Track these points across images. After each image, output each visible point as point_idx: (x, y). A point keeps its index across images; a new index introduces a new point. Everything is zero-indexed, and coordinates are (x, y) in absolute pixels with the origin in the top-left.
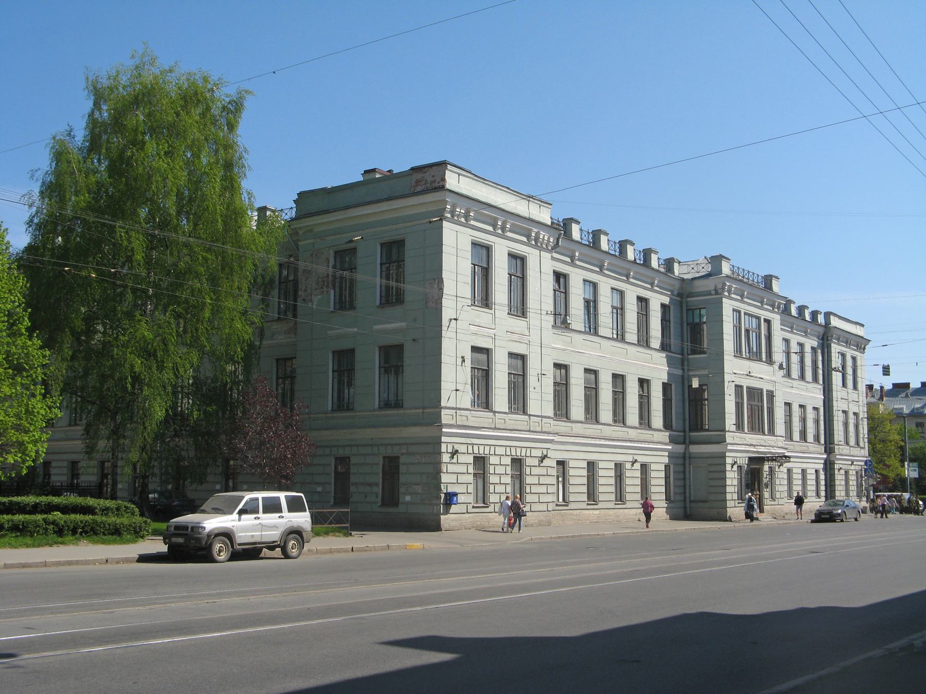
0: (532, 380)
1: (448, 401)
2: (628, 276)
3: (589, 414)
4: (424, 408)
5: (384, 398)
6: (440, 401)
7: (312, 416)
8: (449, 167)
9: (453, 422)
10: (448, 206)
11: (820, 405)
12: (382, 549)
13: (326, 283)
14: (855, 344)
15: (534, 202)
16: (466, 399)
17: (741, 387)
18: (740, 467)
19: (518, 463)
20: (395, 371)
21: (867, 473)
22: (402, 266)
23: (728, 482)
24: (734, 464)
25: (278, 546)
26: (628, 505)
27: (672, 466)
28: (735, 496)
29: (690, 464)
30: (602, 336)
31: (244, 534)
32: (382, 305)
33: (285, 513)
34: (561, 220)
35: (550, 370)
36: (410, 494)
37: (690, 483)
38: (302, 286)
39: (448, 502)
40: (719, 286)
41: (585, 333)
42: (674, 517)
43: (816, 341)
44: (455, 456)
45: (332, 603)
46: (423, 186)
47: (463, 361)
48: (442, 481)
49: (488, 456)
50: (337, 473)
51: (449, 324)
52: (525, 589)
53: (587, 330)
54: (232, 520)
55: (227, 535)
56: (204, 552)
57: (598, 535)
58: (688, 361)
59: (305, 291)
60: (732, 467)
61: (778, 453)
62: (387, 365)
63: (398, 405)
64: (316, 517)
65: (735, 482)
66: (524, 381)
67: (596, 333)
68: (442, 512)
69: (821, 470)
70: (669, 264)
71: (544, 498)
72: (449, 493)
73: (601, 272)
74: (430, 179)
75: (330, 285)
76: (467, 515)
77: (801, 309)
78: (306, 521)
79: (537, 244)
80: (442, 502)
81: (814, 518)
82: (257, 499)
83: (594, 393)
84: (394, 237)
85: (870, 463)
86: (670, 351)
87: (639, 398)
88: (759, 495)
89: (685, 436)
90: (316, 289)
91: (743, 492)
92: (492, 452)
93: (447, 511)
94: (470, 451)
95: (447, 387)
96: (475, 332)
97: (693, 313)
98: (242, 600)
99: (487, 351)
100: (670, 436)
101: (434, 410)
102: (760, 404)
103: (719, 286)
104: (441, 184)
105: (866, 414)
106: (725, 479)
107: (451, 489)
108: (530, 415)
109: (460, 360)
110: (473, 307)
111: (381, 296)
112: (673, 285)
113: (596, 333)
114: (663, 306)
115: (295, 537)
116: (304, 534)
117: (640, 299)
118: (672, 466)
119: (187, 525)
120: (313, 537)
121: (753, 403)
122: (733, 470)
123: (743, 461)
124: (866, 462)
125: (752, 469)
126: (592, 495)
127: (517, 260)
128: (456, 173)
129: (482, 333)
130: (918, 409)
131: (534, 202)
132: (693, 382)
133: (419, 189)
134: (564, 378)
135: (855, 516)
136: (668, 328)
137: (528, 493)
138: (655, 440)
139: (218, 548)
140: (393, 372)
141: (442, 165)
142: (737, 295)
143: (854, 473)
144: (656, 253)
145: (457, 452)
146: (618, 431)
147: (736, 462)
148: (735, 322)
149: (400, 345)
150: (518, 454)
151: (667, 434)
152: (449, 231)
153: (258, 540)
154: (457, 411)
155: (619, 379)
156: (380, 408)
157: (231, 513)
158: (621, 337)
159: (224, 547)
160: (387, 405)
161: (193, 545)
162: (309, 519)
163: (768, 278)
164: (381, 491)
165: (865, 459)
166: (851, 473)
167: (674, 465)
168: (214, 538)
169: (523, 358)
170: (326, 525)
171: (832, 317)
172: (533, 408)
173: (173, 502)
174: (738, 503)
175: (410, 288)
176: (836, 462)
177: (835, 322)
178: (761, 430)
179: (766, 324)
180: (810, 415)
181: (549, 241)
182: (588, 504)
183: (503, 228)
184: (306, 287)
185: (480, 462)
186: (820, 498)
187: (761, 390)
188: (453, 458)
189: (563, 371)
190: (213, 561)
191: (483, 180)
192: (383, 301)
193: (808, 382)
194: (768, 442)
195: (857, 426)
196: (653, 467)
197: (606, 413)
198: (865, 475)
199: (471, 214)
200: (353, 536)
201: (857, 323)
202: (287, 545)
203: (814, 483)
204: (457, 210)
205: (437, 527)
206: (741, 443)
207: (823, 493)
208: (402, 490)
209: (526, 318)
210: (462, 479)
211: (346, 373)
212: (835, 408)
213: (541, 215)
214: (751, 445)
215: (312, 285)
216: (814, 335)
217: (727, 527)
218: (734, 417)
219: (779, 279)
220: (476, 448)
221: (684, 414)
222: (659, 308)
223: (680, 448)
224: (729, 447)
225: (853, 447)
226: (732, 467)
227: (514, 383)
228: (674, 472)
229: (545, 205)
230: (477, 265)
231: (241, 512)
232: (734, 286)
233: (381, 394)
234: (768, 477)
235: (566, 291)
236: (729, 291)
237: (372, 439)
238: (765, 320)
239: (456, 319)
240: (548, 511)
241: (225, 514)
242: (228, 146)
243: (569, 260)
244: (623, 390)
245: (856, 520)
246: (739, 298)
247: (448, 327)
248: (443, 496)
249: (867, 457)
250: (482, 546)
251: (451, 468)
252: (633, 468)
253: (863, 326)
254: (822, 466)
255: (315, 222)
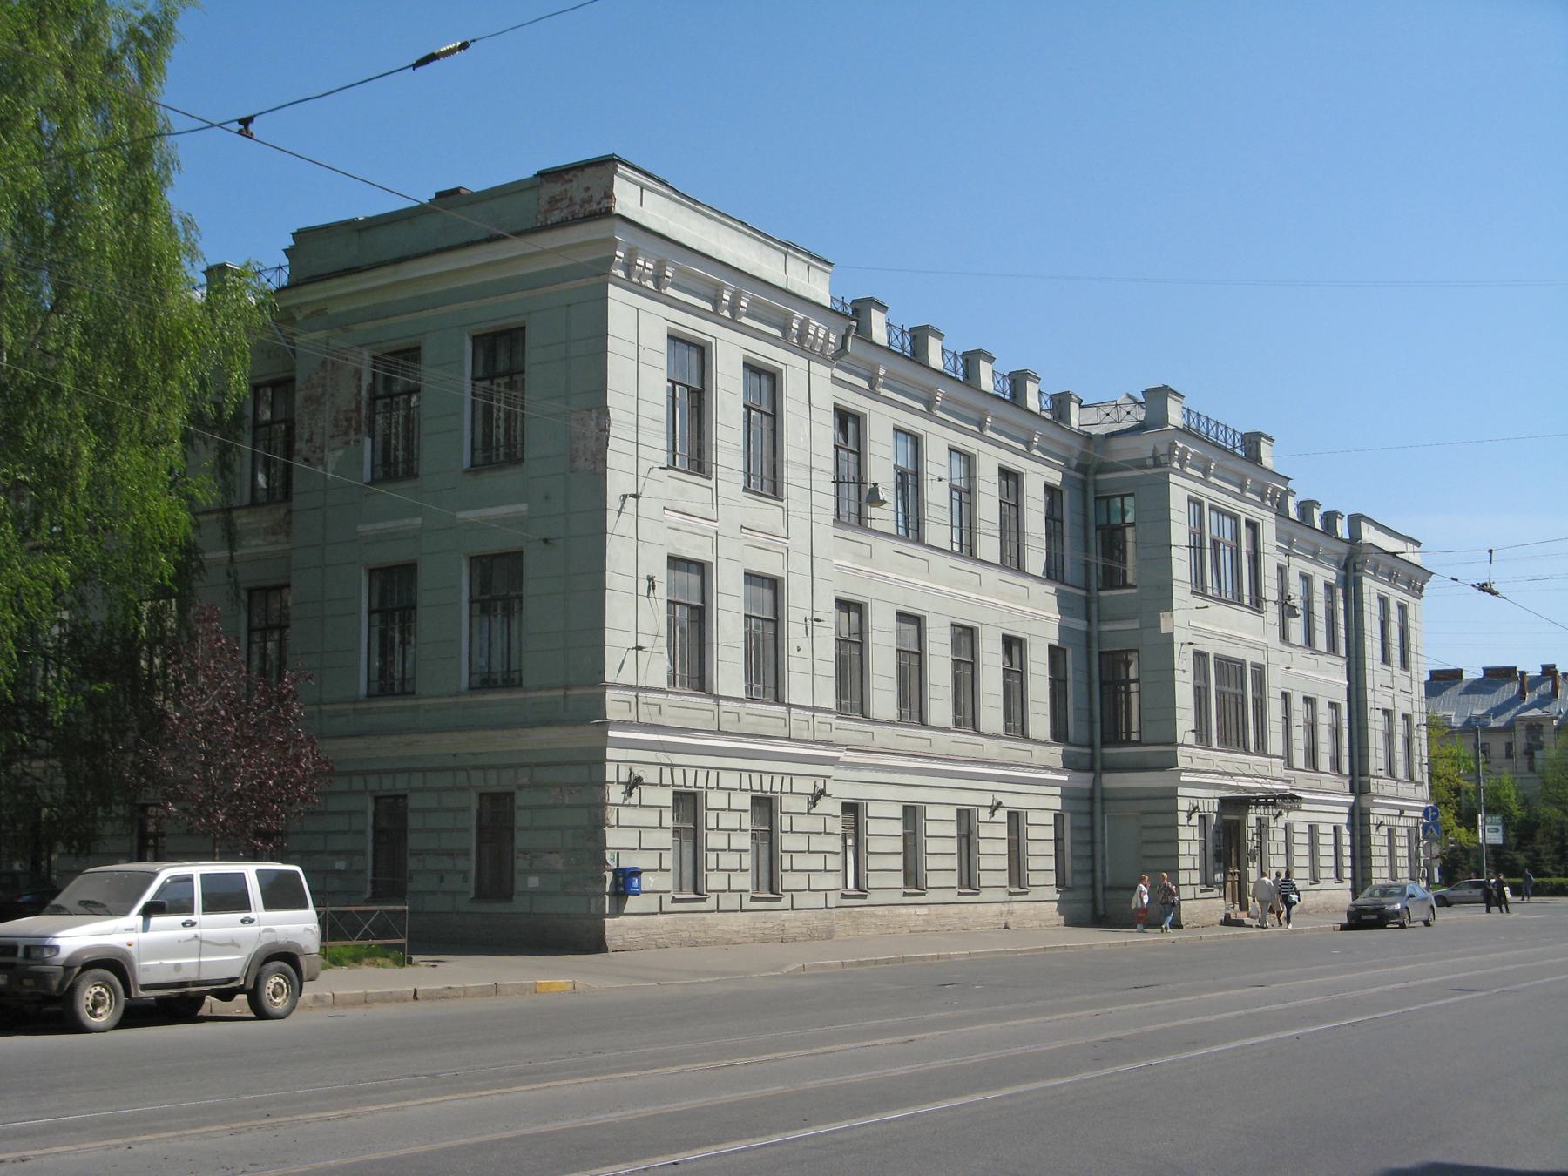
0: (794, 631)
1: (623, 662)
2: (981, 425)
3: (906, 707)
4: (567, 687)
5: (481, 667)
6: (602, 672)
7: (323, 707)
8: (621, 169)
9: (631, 717)
10: (618, 253)
11: (1341, 697)
12: (483, 992)
13: (353, 423)
14: (1406, 579)
15: (797, 258)
16: (657, 670)
17: (1204, 655)
18: (1203, 818)
19: (764, 806)
20: (504, 609)
21: (1428, 833)
22: (519, 385)
23: (1183, 848)
24: (1194, 811)
25: (241, 990)
26: (985, 895)
27: (1068, 817)
28: (1196, 877)
29: (1103, 813)
30: (932, 547)
31: (158, 962)
32: (475, 468)
33: (258, 911)
34: (848, 301)
35: (827, 609)
36: (537, 872)
37: (1103, 850)
38: (302, 431)
39: (622, 889)
40: (1163, 449)
41: (897, 537)
42: (1073, 921)
43: (1333, 570)
44: (635, 791)
45: (372, 1157)
46: (565, 211)
47: (652, 586)
48: (608, 845)
49: (704, 790)
50: (377, 832)
51: (622, 507)
52: (885, 1096)
53: (902, 531)
54: (126, 930)
55: (114, 965)
56: (57, 1008)
57: (939, 957)
58: (1098, 602)
59: (310, 440)
60: (1189, 818)
61: (1277, 790)
62: (487, 597)
63: (511, 681)
64: (332, 925)
65: (1195, 848)
66: (776, 635)
67: (919, 540)
68: (607, 911)
69: (1344, 827)
70: (1060, 404)
71: (820, 881)
72: (624, 871)
73: (929, 414)
74: (579, 195)
75: (364, 428)
76: (662, 918)
77: (1306, 507)
78: (306, 929)
79: (803, 346)
80: (608, 890)
81: (1346, 921)
82: (188, 879)
83: (915, 663)
84: (502, 322)
85: (1435, 814)
86: (1063, 582)
87: (1004, 676)
88: (1239, 876)
89: (1092, 755)
90: (332, 437)
91: (1210, 869)
92: (712, 783)
93: (618, 909)
94: (667, 780)
95: (617, 640)
96: (676, 526)
97: (1108, 503)
98: (108, 1148)
99: (701, 568)
100: (1065, 756)
101: (590, 691)
102: (1239, 691)
103: (1163, 449)
104: (605, 204)
105: (1425, 716)
106: (1175, 841)
107: (627, 862)
108: (790, 706)
109: (644, 585)
110: (671, 472)
111: (473, 450)
112: (1069, 448)
113: (919, 540)
114: (1049, 489)
115: (281, 967)
116: (303, 961)
117: (1005, 473)
118: (1068, 817)
119: (15, 942)
120: (324, 968)
121: (1225, 688)
122: (1190, 823)
123: (1210, 807)
124: (1426, 812)
125: (1225, 821)
126: (914, 877)
127: (763, 377)
128: (635, 183)
129: (689, 529)
130: (1478, 718)
131: (797, 258)
132: (1162, 620)
133: (556, 216)
134: (855, 629)
135: (1424, 917)
136: (1058, 534)
137: (787, 871)
138: (1036, 762)
139: (91, 997)
140: (499, 611)
141: (606, 164)
142: (1197, 469)
143: (1405, 833)
144: (1036, 380)
145: (639, 781)
146: (963, 743)
147: (1197, 807)
148: (1192, 525)
149: (514, 553)
150: (767, 787)
151: (1059, 750)
152: (622, 306)
153: (192, 976)
154: (640, 694)
155: (965, 636)
156: (471, 688)
157: (125, 912)
158: (968, 550)
159: (107, 995)
160: (485, 682)
161: (27, 991)
162: (314, 926)
163: (1253, 439)
164: (474, 866)
165: (1423, 805)
166: (1398, 831)
167: (1073, 813)
168: (81, 972)
169: (774, 584)
170: (355, 942)
171: (1363, 524)
172: (796, 689)
173: (20, 896)
174: (1202, 891)
175: (538, 443)
176: (1373, 811)
177: (1369, 534)
178: (1241, 743)
179: (1249, 530)
180: (1324, 717)
181: (826, 340)
182: (905, 894)
183: (734, 307)
184: (312, 434)
185: (688, 803)
186: (1342, 882)
187: (1243, 663)
188: (630, 795)
189: (854, 616)
190: (80, 1028)
191: (691, 201)
192: (479, 460)
193: (1321, 653)
194: (1256, 768)
195: (1408, 741)
196: (1033, 817)
197: (940, 708)
198: (1425, 837)
199: (667, 273)
200: (416, 965)
201: (1407, 539)
202: (261, 987)
203: (1331, 851)
204: (639, 262)
205: (596, 944)
206: (1205, 768)
207: (1347, 873)
208: (521, 863)
209: (782, 500)
210: (650, 839)
211: (397, 613)
212: (1370, 705)
213: (812, 286)
214: (1225, 774)
215: (323, 428)
216: (1331, 561)
217: (1187, 940)
218: (1191, 715)
219: (1273, 440)
220: (678, 773)
221: (1091, 710)
222: (1040, 494)
223: (1084, 780)
224: (1185, 778)
225: (1402, 781)
226: (1189, 818)
227: (757, 637)
228: (1073, 828)
229: (819, 265)
230: (679, 384)
231: (150, 910)
232: (1191, 449)
233: (474, 657)
234: (1255, 838)
235: (859, 449)
236: (1182, 462)
237: (454, 755)
238: (1249, 523)
239: (636, 496)
240: (827, 908)
241: (111, 915)
242: (137, 112)
243: (864, 384)
244: (973, 658)
245: (1427, 923)
246: (1200, 475)
247: (620, 512)
248: (609, 876)
249: (1427, 802)
250: (701, 982)
251: (627, 816)
252: (993, 820)
253: (1418, 544)
254: (1345, 819)
255: (330, 294)
